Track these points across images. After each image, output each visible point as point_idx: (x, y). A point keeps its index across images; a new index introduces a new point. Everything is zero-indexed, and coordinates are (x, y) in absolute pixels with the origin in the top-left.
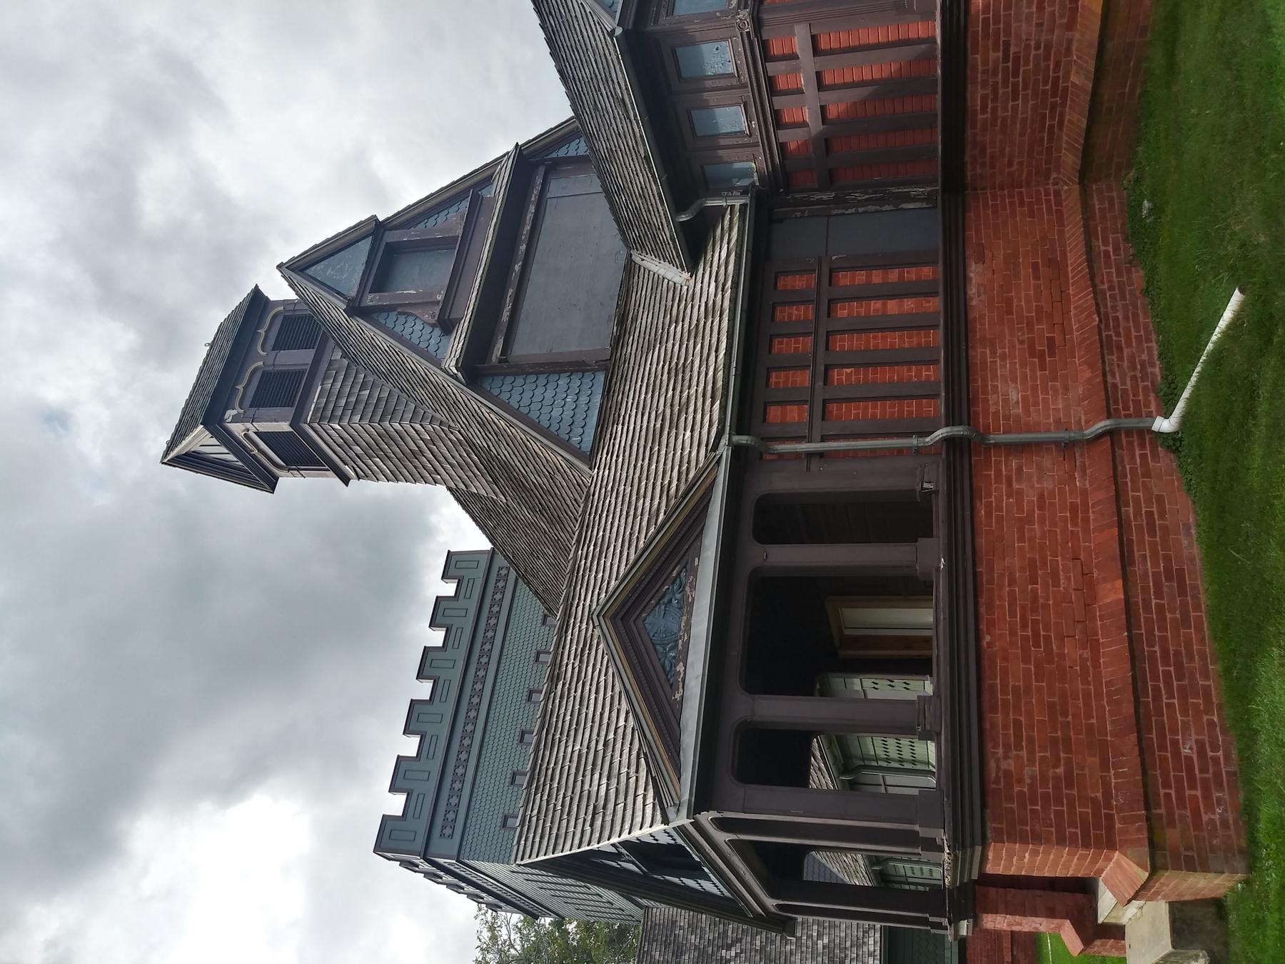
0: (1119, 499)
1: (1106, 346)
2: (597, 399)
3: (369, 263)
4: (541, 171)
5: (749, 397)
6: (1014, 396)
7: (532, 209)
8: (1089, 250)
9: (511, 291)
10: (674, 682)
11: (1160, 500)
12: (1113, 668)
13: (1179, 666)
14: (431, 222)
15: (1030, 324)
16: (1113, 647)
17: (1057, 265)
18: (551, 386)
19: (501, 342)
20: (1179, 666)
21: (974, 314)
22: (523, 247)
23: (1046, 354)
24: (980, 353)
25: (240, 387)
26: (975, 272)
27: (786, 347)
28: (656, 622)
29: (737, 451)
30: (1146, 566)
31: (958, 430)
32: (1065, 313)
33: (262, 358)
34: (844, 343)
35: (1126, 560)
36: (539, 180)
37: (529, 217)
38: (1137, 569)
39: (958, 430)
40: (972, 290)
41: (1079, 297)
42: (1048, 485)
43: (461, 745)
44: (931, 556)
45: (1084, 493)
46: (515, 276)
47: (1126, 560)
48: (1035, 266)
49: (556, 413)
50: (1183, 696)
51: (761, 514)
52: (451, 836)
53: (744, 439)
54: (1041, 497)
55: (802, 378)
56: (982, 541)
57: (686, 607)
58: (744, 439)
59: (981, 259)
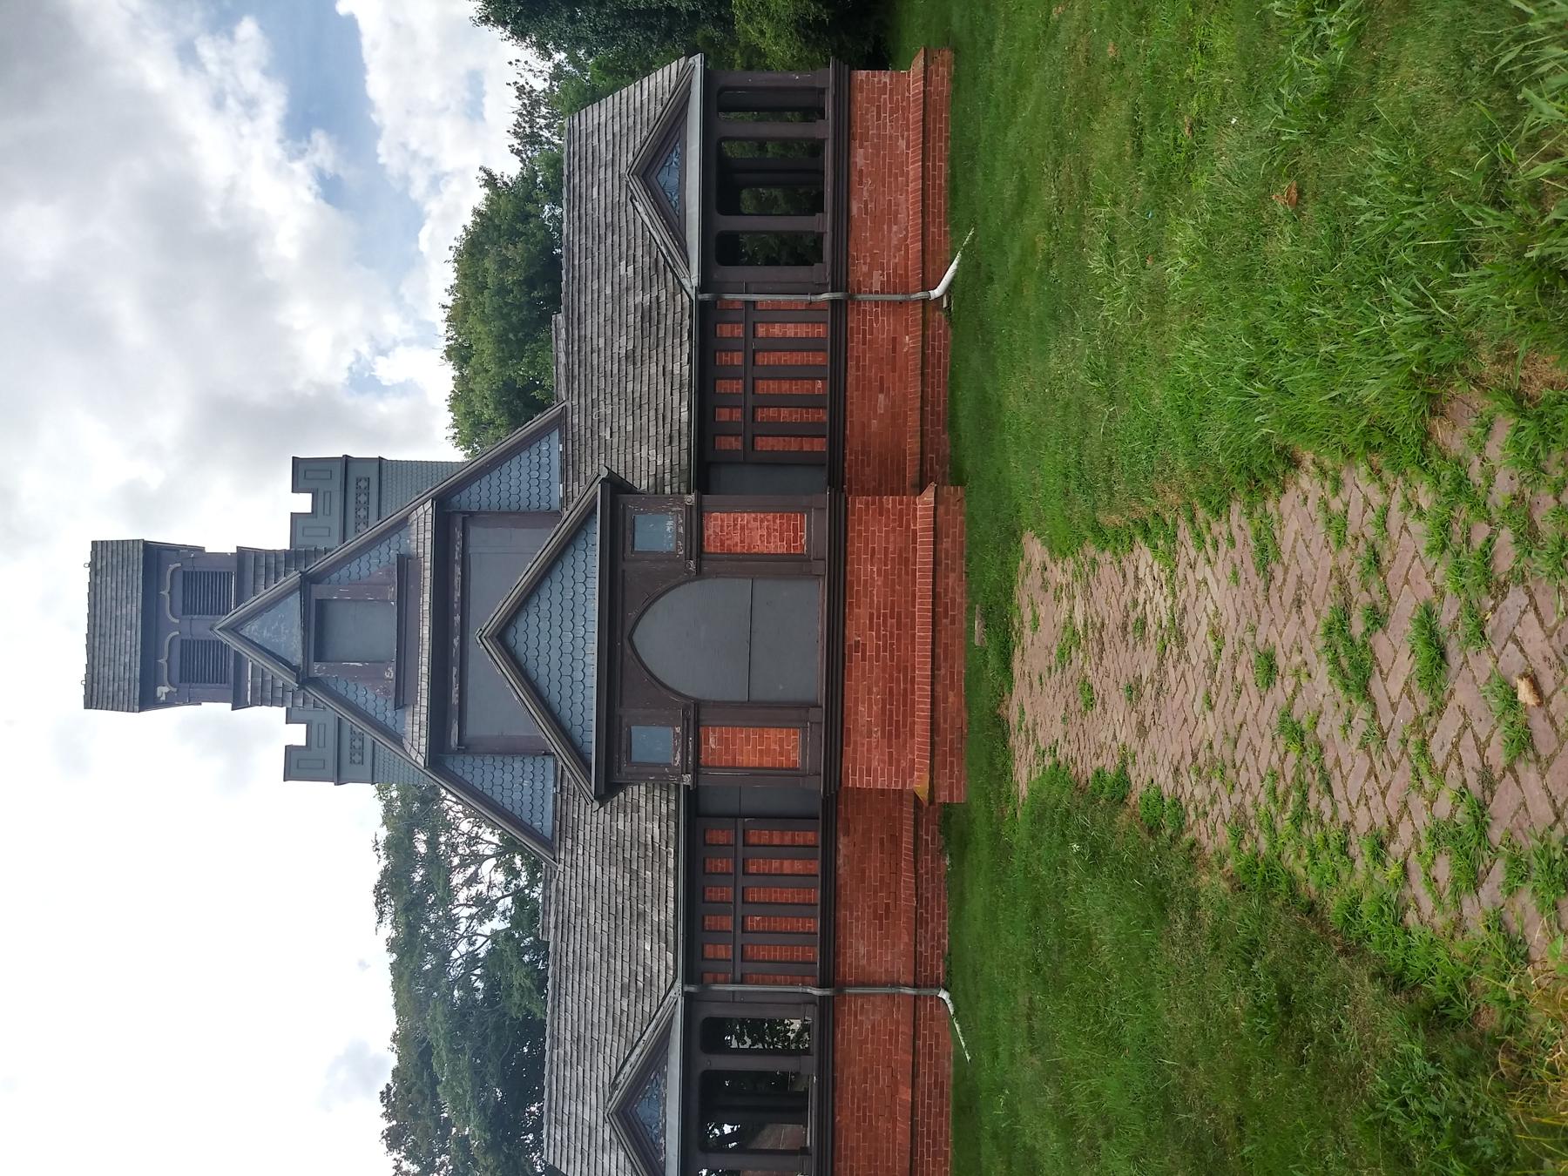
0: (915, 1037)
1: (919, 922)
2: (551, 790)
3: (305, 628)
4: (459, 519)
5: (693, 969)
6: (862, 950)
7: (458, 570)
8: (916, 837)
9: (455, 670)
10: (659, 1150)
11: (937, 1035)
12: (903, 1138)
13: (934, 1140)
14: (354, 566)
15: (875, 892)
16: (903, 1126)
17: (895, 840)
18: (508, 768)
19: (456, 727)
20: (934, 1140)
21: (841, 882)
22: (457, 618)
23: (883, 916)
24: (843, 914)
25: (165, 593)
26: (842, 841)
27: (724, 386)
28: (667, 178)
29: (687, 996)
30: (925, 1080)
31: (838, 295)
32: (898, 883)
33: (175, 627)
34: (763, 359)
35: (915, 1076)
36: (459, 535)
37: (457, 580)
38: (920, 1080)
39: (838, 295)
40: (840, 861)
41: (907, 877)
42: (878, 1017)
43: (357, 516)
44: (824, 223)
45: (898, 1022)
46: (455, 651)
47: (915, 1076)
48: (882, 843)
49: (517, 796)
50: (935, 1155)
51: (706, 1032)
52: (359, 480)
53: (692, 989)
54: (873, 1027)
55: (737, 386)
56: (838, 1056)
57: (661, 1100)
58: (692, 989)
59: (847, 834)
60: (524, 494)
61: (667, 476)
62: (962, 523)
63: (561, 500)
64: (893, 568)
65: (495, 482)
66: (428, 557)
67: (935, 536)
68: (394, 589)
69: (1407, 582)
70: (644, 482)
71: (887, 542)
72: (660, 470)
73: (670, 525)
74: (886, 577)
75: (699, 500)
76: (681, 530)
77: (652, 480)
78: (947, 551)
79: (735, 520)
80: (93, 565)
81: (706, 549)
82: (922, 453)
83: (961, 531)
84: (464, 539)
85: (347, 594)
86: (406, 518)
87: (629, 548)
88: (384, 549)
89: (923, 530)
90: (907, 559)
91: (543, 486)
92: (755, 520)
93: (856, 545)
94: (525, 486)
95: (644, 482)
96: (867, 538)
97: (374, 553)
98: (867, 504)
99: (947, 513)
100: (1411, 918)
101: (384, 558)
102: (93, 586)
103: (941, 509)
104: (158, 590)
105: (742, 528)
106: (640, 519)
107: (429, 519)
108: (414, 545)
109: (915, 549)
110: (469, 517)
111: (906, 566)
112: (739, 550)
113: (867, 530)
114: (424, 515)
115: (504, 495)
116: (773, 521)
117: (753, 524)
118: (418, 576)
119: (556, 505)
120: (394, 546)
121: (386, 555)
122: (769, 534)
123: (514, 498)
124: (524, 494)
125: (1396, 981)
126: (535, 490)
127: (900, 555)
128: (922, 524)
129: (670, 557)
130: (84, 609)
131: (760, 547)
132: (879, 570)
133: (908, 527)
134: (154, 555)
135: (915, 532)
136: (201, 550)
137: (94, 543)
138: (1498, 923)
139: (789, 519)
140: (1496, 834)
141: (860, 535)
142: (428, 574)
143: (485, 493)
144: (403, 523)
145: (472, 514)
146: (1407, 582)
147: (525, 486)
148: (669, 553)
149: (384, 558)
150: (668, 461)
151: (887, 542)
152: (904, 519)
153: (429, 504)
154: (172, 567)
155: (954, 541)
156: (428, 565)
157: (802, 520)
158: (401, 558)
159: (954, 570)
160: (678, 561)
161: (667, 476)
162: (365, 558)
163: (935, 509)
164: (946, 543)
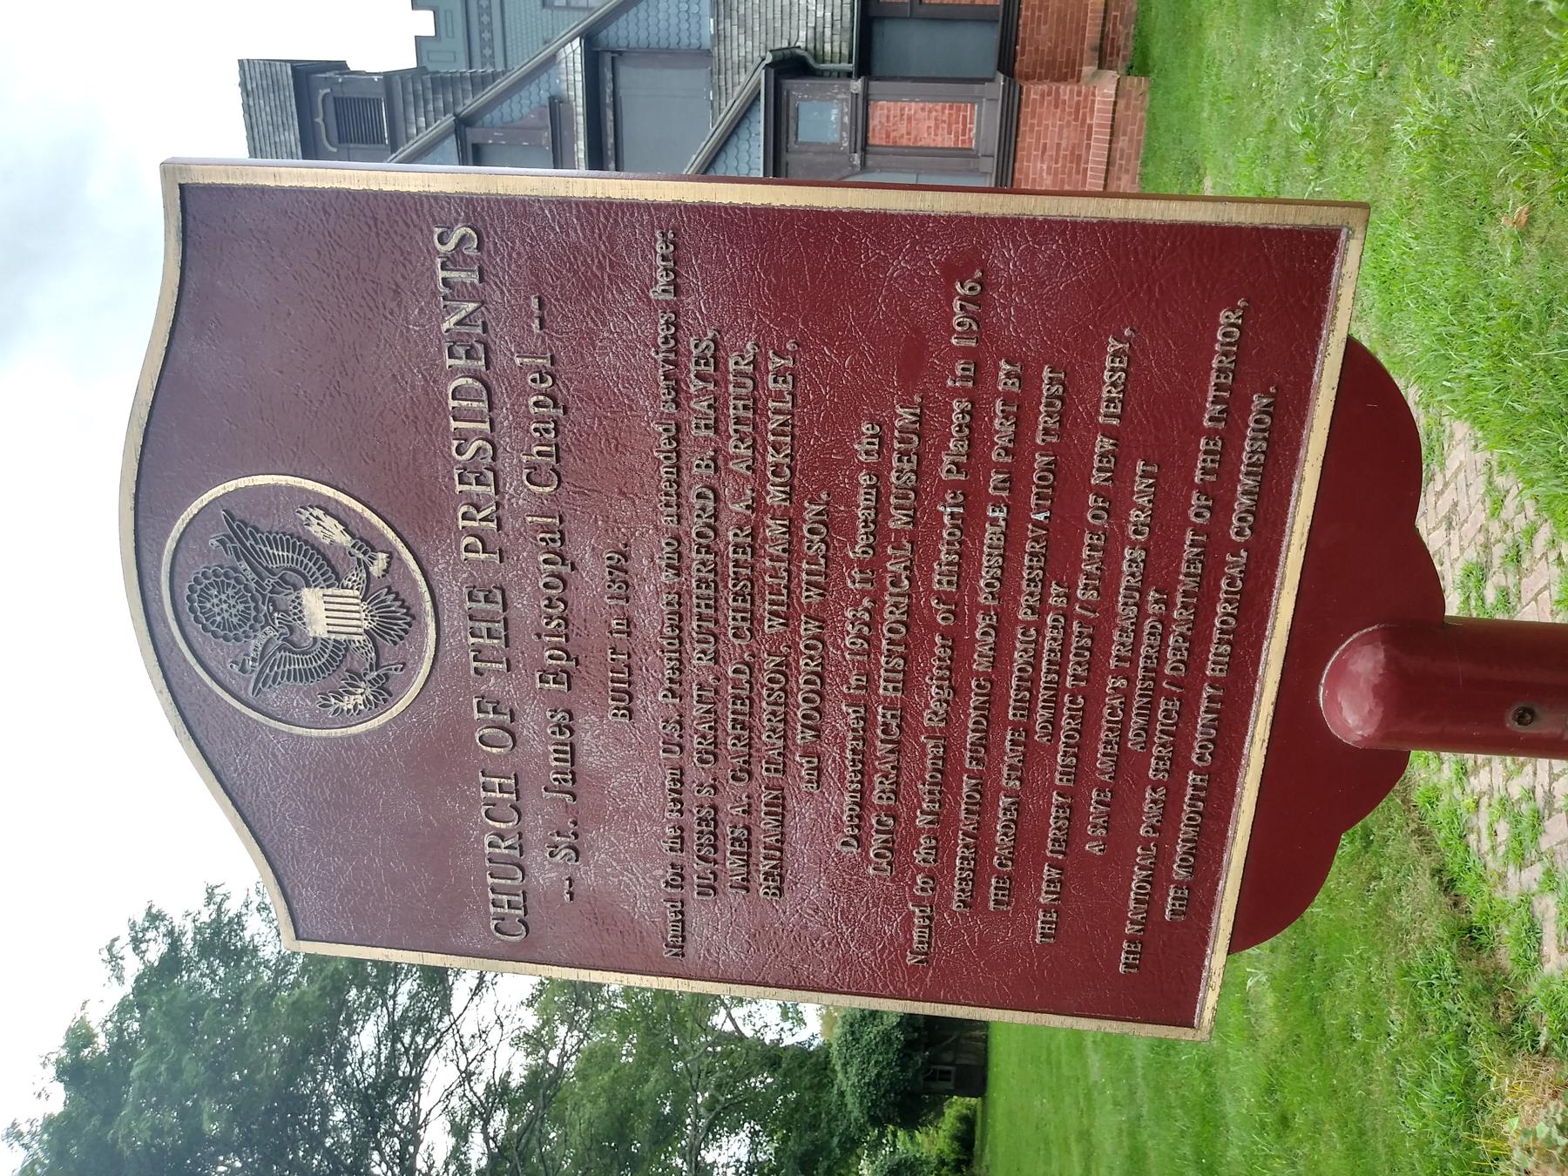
4: (608, 58)
7: (610, 114)
14: (505, 107)
25: (319, 120)
36: (609, 75)
37: (610, 125)
60: (673, 30)
61: (828, 32)
62: (1142, 119)
63: (712, 37)
64: (1064, 166)
65: (642, 15)
66: (580, 101)
67: (1112, 134)
68: (547, 134)
69: (1535, 599)
70: (802, 34)
71: (1060, 137)
72: (820, 22)
73: (834, 114)
74: (1056, 174)
75: (866, 87)
76: (846, 119)
77: (811, 32)
78: (1122, 151)
79: (902, 109)
80: (243, 84)
81: (871, 141)
82: (1106, 11)
83: (1140, 128)
84: (614, 80)
85: (502, 138)
86: (553, 57)
87: (792, 138)
88: (533, 88)
89: (1099, 125)
90: (1079, 156)
91: (693, 21)
92: (923, 109)
93: (1027, 140)
94: (674, 21)
95: (802, 34)
96: (1039, 132)
97: (524, 93)
98: (1043, 96)
99: (1127, 107)
100: (1472, 838)
101: (534, 98)
102: (247, 109)
103: (1121, 104)
104: (312, 118)
105: (909, 119)
106: (804, 108)
107: (578, 59)
108: (564, 86)
109: (1088, 146)
110: (618, 55)
111: (1078, 164)
112: (904, 142)
113: (1039, 125)
114: (573, 54)
115: (653, 30)
116: (942, 111)
117: (922, 115)
118: (572, 121)
119: (707, 43)
120: (544, 86)
121: (537, 94)
122: (937, 127)
123: (663, 34)
124: (673, 30)
125: (1447, 885)
126: (684, 26)
127: (1073, 153)
128: (1099, 118)
129: (834, 149)
130: (242, 132)
131: (927, 140)
132: (1049, 168)
133: (1084, 120)
134: (305, 75)
135: (1090, 127)
136: (341, 66)
137: (241, 62)
138: (1526, 901)
139: (959, 110)
140: (1544, 844)
141: (1032, 130)
142: (581, 119)
143: (632, 26)
144: (552, 59)
145: (620, 53)
146: (1535, 599)
147: (674, 21)
148: (833, 144)
149: (534, 98)
150: (828, 14)
151: (1060, 137)
152: (1080, 111)
153: (576, 43)
154: (322, 92)
155: (1131, 140)
156: (580, 110)
157: (972, 112)
158: (552, 99)
159: (1127, 171)
160: (843, 153)
161: (828, 32)
162: (515, 98)
163: (1115, 103)
164: (1122, 142)
